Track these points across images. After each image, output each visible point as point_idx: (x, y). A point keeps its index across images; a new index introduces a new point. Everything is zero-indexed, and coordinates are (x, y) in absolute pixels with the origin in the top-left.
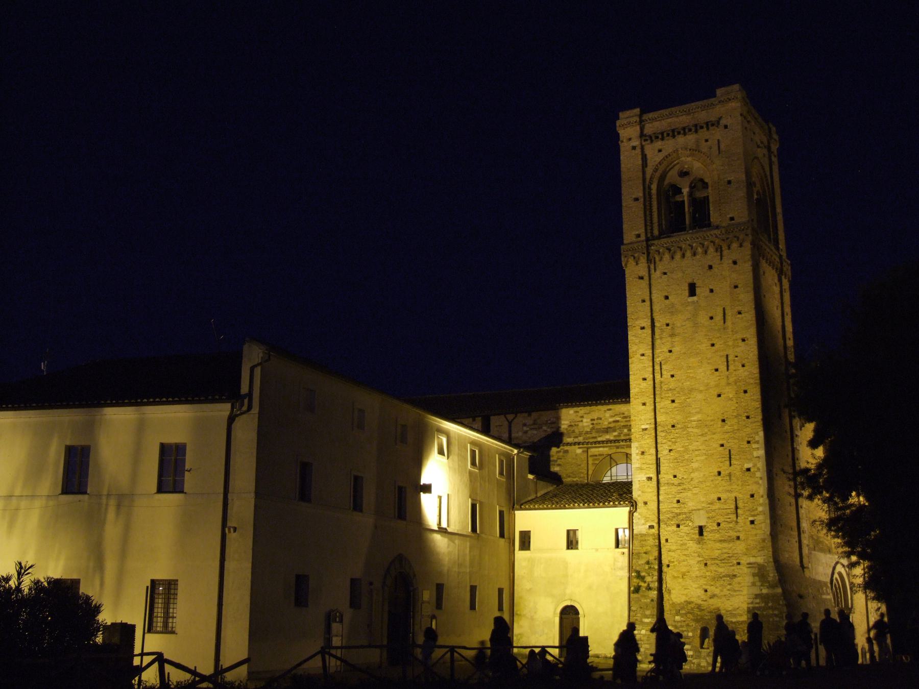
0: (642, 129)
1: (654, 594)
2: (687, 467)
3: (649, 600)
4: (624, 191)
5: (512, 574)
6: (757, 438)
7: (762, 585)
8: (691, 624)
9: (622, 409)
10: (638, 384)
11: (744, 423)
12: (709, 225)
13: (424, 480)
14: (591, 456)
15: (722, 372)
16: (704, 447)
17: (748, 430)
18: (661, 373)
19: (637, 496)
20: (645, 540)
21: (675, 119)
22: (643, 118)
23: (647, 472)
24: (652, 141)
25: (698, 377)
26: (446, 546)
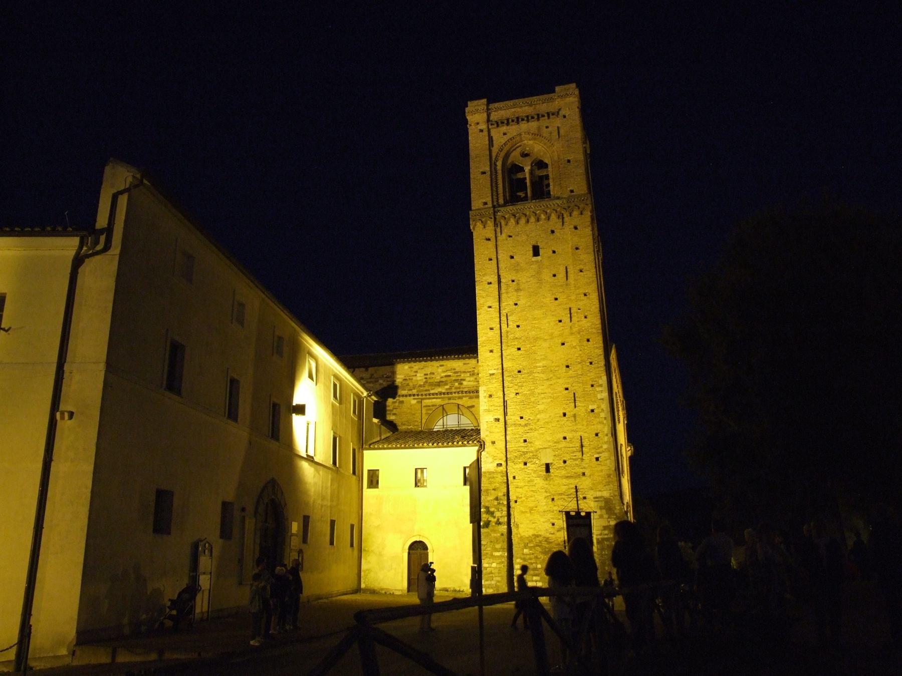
0: (489, 116)
1: (504, 528)
2: (533, 409)
3: (499, 535)
4: (472, 165)
5: (360, 512)
6: (601, 382)
7: (609, 518)
8: (539, 557)
9: (454, 365)
10: (486, 334)
11: (588, 369)
12: (548, 196)
13: (297, 401)
14: (424, 406)
15: (565, 323)
16: (550, 390)
17: (592, 375)
18: (508, 324)
19: (485, 436)
20: (494, 478)
21: (519, 110)
22: (490, 107)
23: (495, 413)
24: (498, 126)
25: (542, 328)
26: (313, 475)
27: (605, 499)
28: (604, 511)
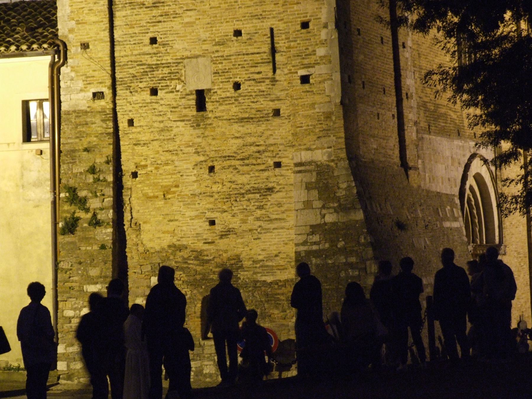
3: (96, 247)
19: (66, 32)
27: (318, 166)
28: (315, 193)
